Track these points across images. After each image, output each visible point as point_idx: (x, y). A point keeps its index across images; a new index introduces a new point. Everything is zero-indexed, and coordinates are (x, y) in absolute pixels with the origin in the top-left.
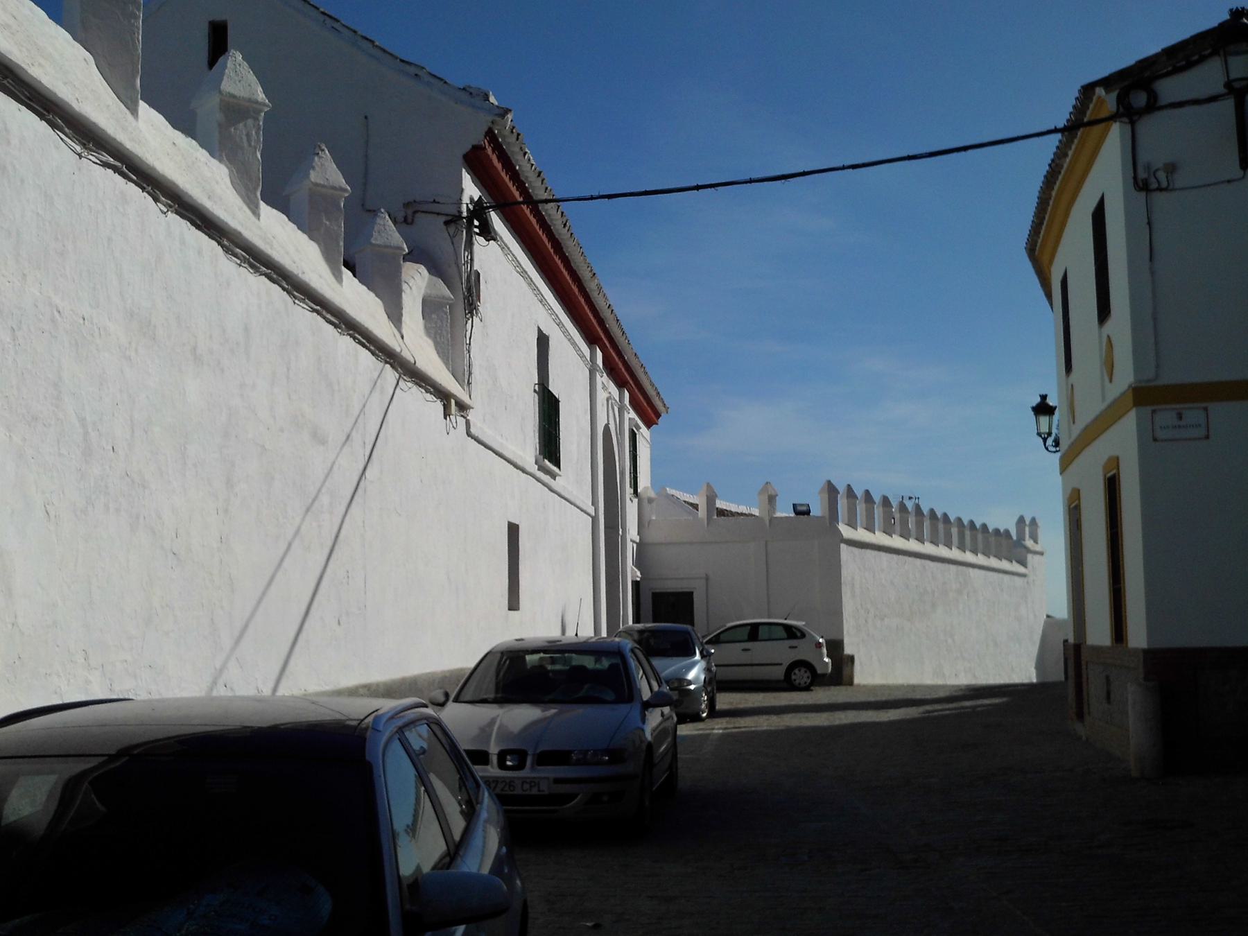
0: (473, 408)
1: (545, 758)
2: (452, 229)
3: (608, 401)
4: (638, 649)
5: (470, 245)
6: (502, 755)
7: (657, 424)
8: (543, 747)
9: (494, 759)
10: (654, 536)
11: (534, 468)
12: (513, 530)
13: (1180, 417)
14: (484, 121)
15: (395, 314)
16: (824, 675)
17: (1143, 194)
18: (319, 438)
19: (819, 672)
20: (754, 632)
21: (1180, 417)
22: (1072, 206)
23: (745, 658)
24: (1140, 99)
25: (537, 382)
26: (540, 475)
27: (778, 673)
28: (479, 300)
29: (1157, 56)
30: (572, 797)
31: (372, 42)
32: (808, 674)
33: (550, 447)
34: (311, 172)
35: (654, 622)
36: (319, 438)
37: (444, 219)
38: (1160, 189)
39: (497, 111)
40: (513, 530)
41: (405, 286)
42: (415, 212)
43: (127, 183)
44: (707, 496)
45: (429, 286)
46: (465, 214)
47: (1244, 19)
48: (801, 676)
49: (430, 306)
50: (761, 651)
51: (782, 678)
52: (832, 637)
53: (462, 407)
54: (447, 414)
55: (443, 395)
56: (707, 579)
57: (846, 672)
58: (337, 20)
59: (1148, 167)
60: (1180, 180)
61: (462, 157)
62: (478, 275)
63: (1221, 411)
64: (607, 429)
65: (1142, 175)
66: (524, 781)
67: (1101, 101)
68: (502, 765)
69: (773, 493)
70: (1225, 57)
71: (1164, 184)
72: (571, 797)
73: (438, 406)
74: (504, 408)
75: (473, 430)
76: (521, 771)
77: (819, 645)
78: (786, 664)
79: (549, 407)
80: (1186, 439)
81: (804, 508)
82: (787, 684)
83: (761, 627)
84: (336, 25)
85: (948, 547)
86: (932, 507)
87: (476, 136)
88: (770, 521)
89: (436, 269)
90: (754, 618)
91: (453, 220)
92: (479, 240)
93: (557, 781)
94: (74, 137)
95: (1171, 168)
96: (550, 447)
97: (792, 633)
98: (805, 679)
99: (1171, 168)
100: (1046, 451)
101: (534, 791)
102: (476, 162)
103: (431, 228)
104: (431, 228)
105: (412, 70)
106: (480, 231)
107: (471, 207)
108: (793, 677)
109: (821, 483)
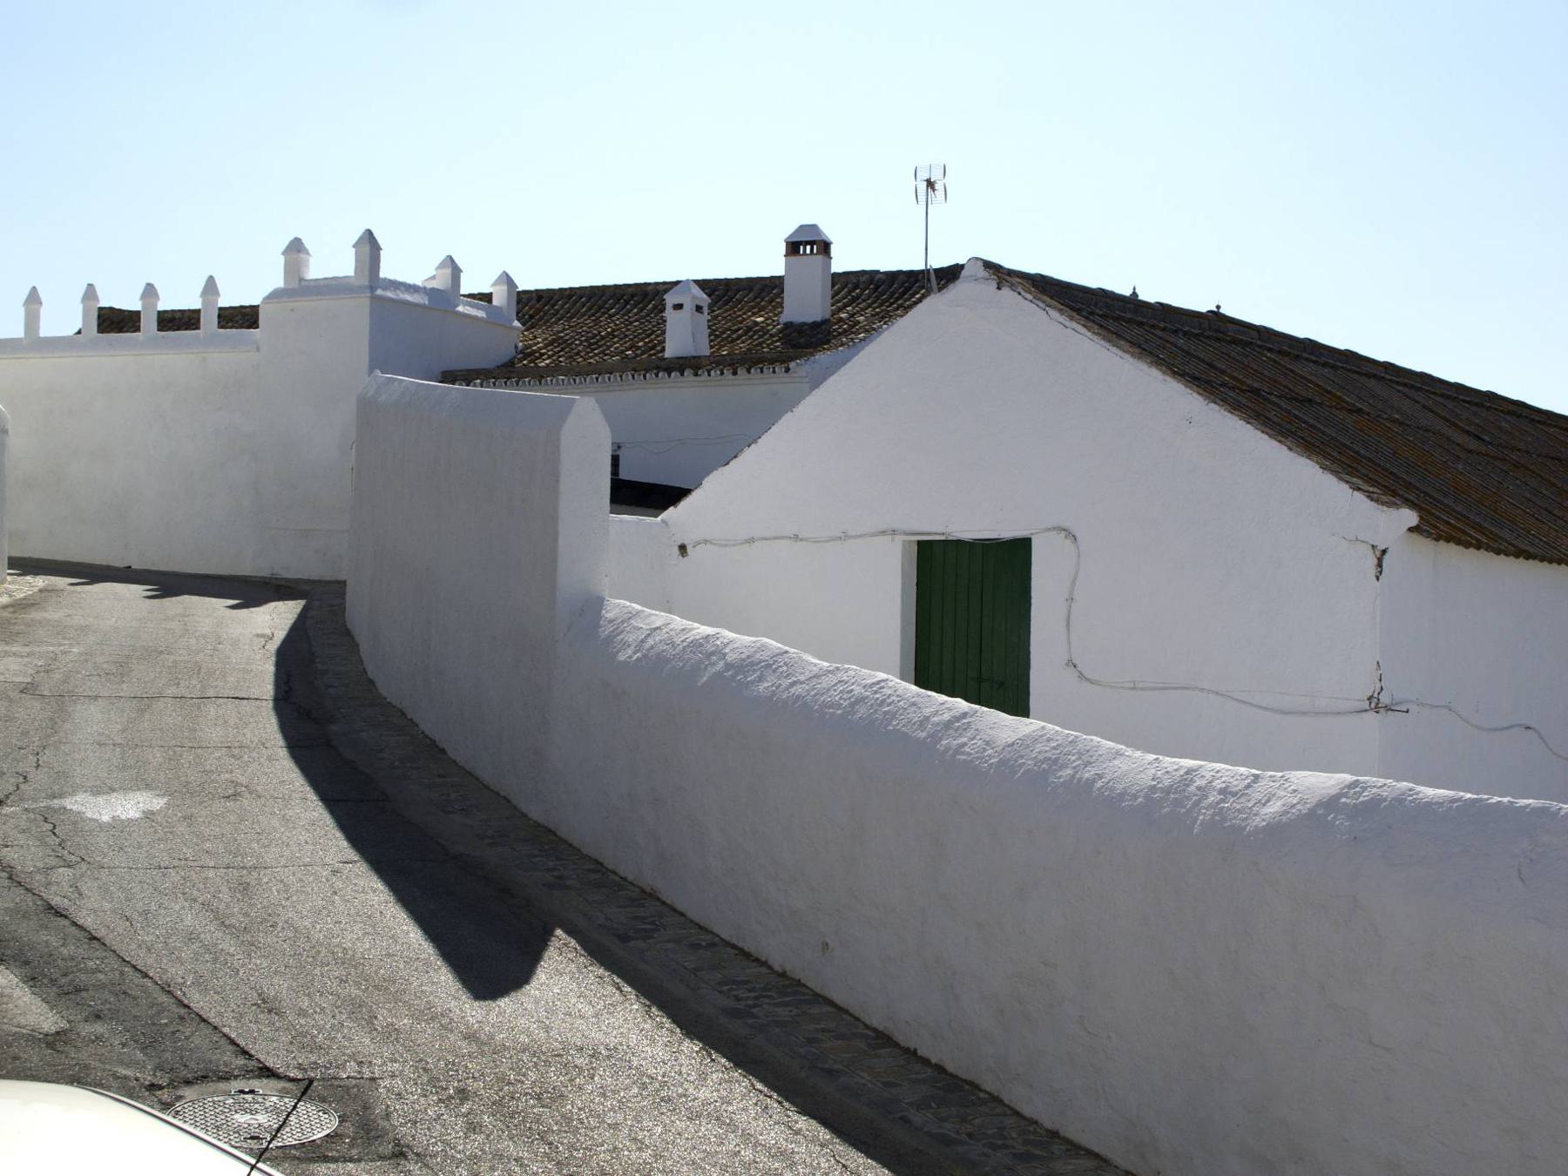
0: (1411, 530)
4: (1488, 799)
7: (507, 279)
19: (279, 282)
22: (31, 1080)
25: (1221, 311)
34: (1410, 517)
35: (575, 399)
43: (1218, 307)
45: (609, 417)
47: (484, 316)
51: (520, 289)
61: (808, 220)
67: (163, 1094)
74: (1381, 664)
76: (464, 996)
80: (927, 199)
83: (624, 474)
85: (1051, 1131)
86: (368, 228)
94: (1039, 299)
100: (1065, 524)
106: (487, 314)
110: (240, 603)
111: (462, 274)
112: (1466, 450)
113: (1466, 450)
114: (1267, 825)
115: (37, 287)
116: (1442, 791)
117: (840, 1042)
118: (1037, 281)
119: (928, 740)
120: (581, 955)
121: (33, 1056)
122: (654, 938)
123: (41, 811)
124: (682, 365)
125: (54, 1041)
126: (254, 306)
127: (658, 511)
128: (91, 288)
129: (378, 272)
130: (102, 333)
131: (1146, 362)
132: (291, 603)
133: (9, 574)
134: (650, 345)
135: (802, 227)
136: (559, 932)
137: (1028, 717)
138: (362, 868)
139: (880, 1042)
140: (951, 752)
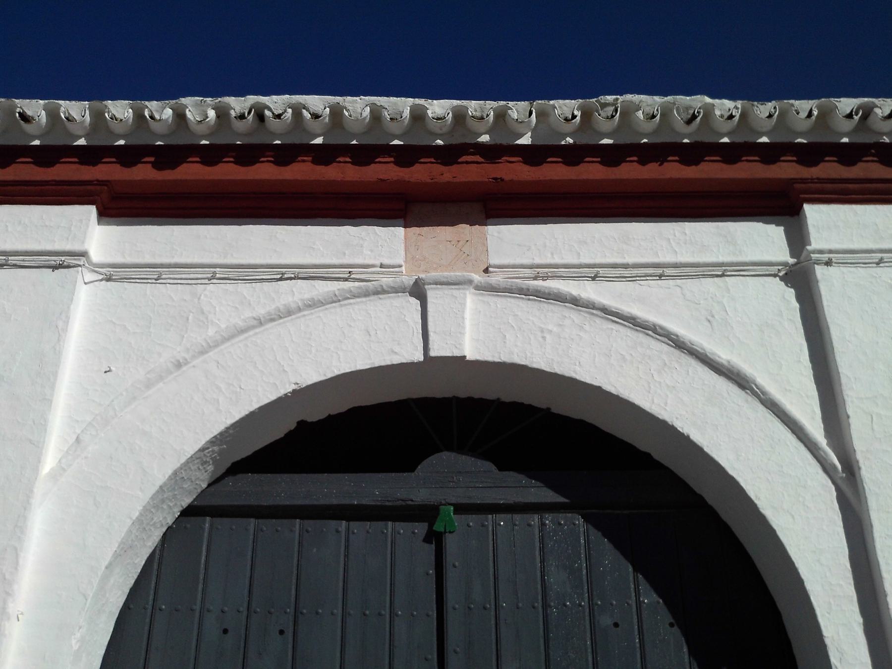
111: (331, 414)
112: (711, 325)
113: (711, 325)
114: (214, 446)
116: (866, 99)
117: (659, 254)
119: (350, 155)
120: (839, 352)
123: (198, 456)
125: (304, 108)
127: (802, 210)
129: (412, 364)
131: (640, 319)
133: (400, 266)
135: (302, 424)
138: (353, 369)
139: (494, 181)
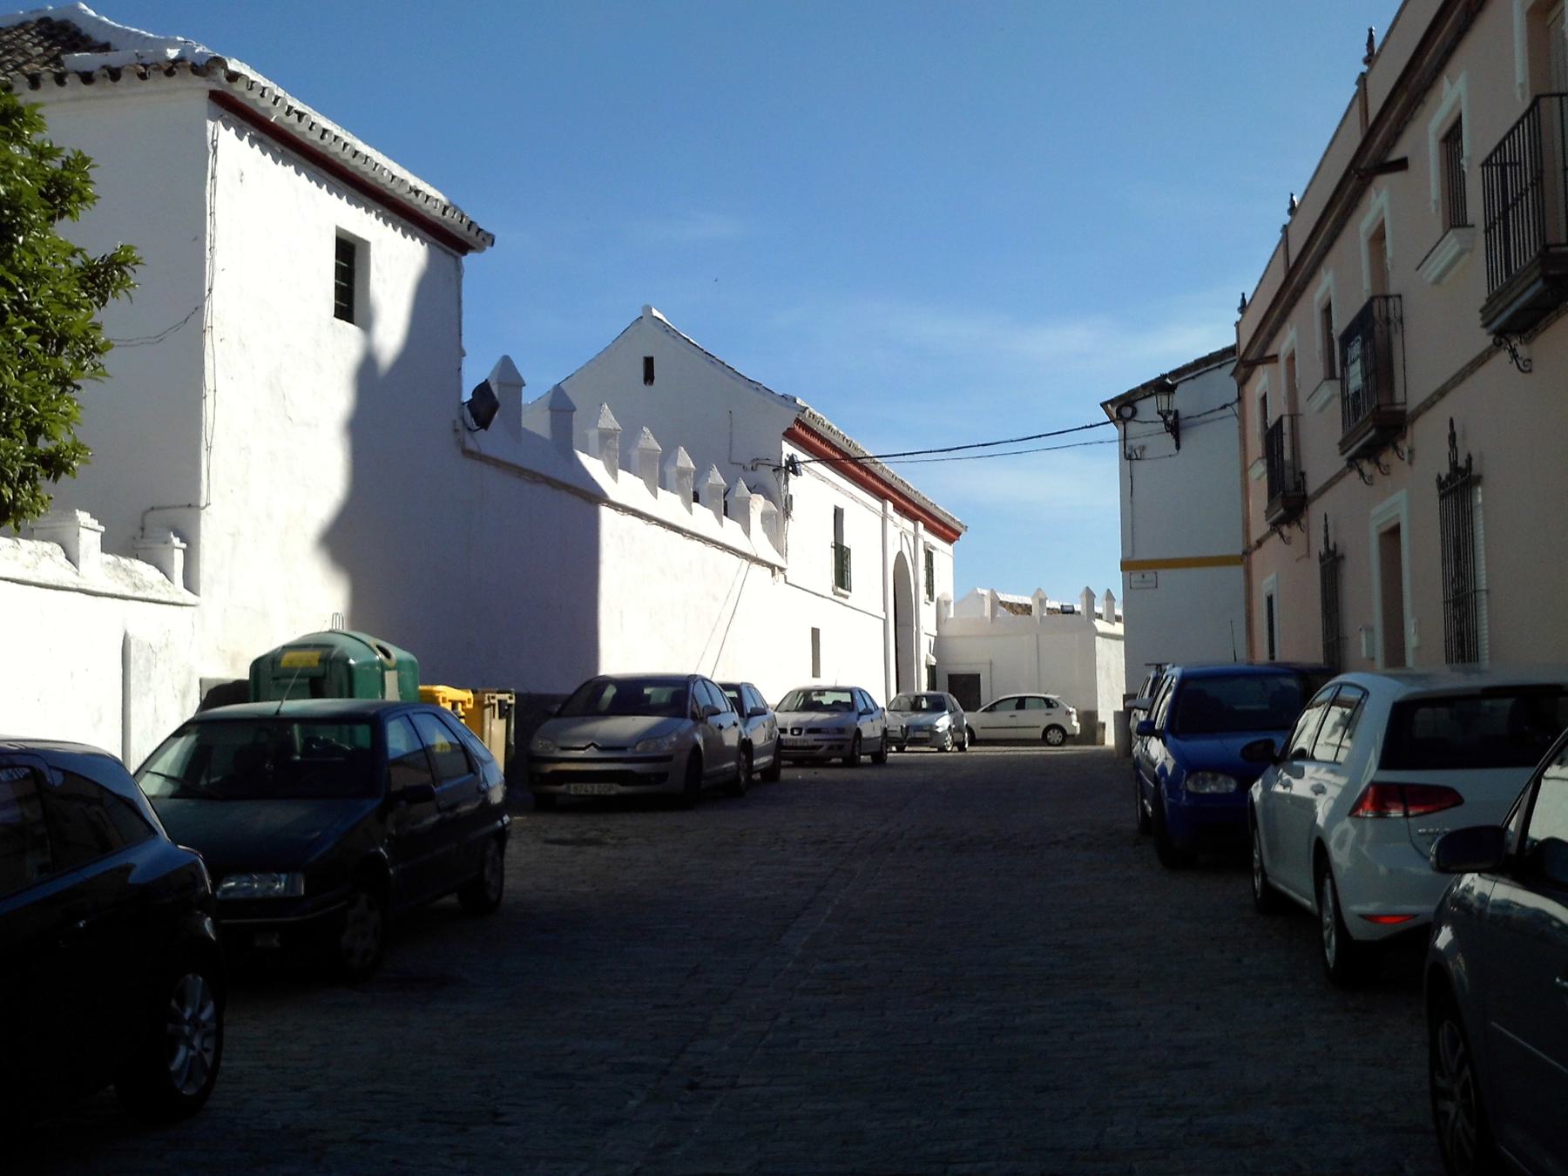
1: (810, 731)
2: (777, 474)
3: (901, 534)
5: (787, 480)
6: (792, 730)
8: (809, 727)
9: (789, 731)
10: (948, 630)
11: (831, 594)
12: (815, 633)
13: (1143, 576)
14: (794, 415)
15: (747, 531)
16: (1073, 736)
17: (1129, 461)
18: (715, 599)
19: (1068, 733)
20: (1021, 703)
21: (1143, 576)
23: (1013, 722)
24: (1127, 412)
26: (836, 598)
27: (1038, 734)
28: (791, 509)
29: (1138, 388)
30: (821, 747)
31: (733, 369)
32: (1061, 734)
33: (842, 577)
36: (715, 599)
37: (772, 468)
38: (1137, 459)
39: (800, 409)
40: (815, 633)
41: (751, 509)
42: (757, 465)
44: (991, 600)
45: (765, 505)
46: (784, 465)
48: (1054, 736)
49: (765, 517)
50: (1024, 717)
52: (1087, 707)
53: (781, 569)
54: (773, 574)
55: (772, 567)
56: (991, 664)
57: (1099, 734)
58: (714, 357)
59: (1131, 448)
60: (1147, 454)
62: (791, 497)
63: (1163, 574)
64: (900, 556)
65: (1128, 452)
66: (801, 740)
68: (792, 733)
69: (1043, 597)
70: (1124, 424)
71: (1139, 456)
72: (821, 747)
73: (769, 571)
75: (788, 581)
77: (1069, 713)
78: (1044, 727)
79: (842, 556)
81: (1070, 609)
82: (1044, 740)
83: (1027, 700)
84: (714, 360)
87: (790, 423)
88: (1041, 620)
89: (769, 496)
90: (1029, 692)
91: (777, 469)
92: (791, 475)
93: (815, 740)
95: (1143, 448)
96: (842, 577)
97: (1049, 704)
98: (1058, 738)
99: (1143, 448)
101: (806, 744)
102: (790, 436)
103: (766, 474)
104: (766, 474)
105: (755, 386)
107: (788, 459)
108: (1048, 737)
109: (1082, 589)
110: (1328, 965)
115: (513, 358)
118: (197, 67)
121: (1435, 398)
122: (948, 752)
124: (924, 710)
126: (483, 383)
128: (1039, 589)
130: (1303, 775)
132: (1273, 422)
134: (22, 31)
136: (645, 429)
137: (1097, 711)
140: (1470, 1081)
